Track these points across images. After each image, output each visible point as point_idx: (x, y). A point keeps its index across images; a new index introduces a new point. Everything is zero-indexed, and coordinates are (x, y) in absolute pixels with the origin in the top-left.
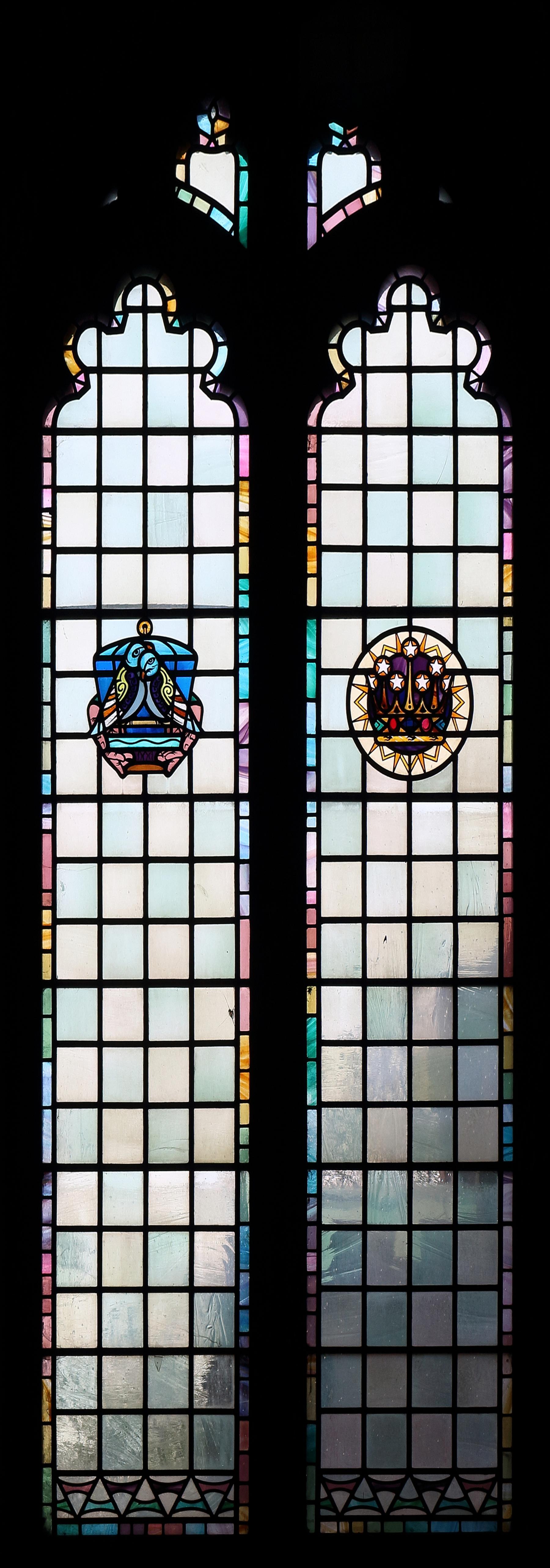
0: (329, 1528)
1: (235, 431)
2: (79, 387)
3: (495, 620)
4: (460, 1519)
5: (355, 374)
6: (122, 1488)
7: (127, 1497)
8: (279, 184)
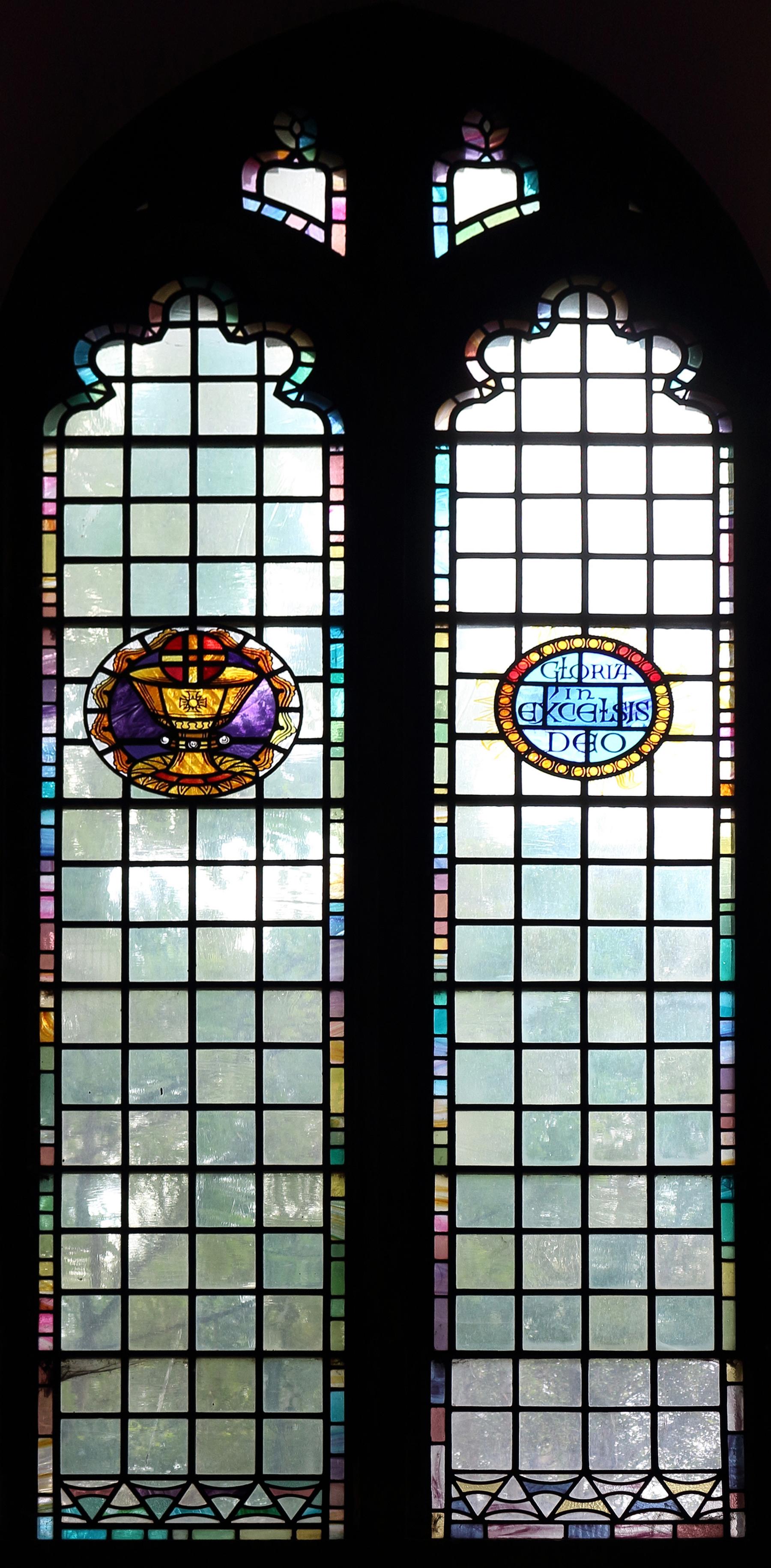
1: (714, 440)
7: (167, 1502)
8: (389, 202)
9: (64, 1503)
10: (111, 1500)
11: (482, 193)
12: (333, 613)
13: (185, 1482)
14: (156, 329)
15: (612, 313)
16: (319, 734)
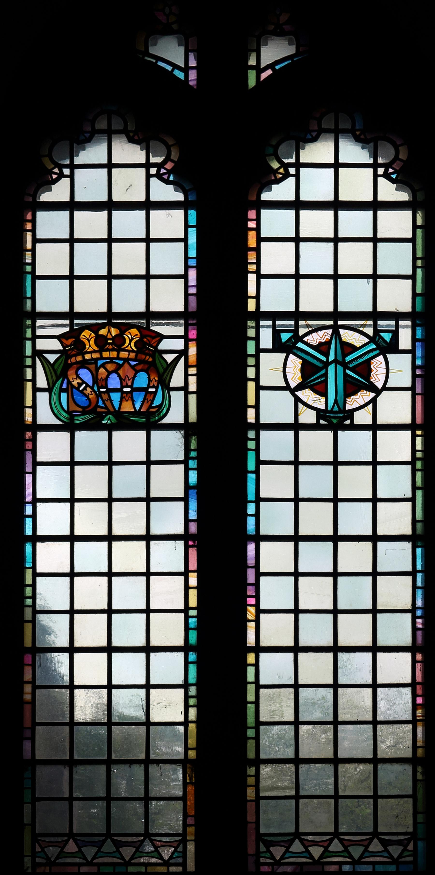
0: (265, 869)
4: (340, 864)
7: (400, 848)
8: (223, 57)
9: (261, 850)
10: (368, 848)
11: (273, 52)
12: (190, 310)
14: (87, 135)
15: (354, 125)
16: (182, 384)
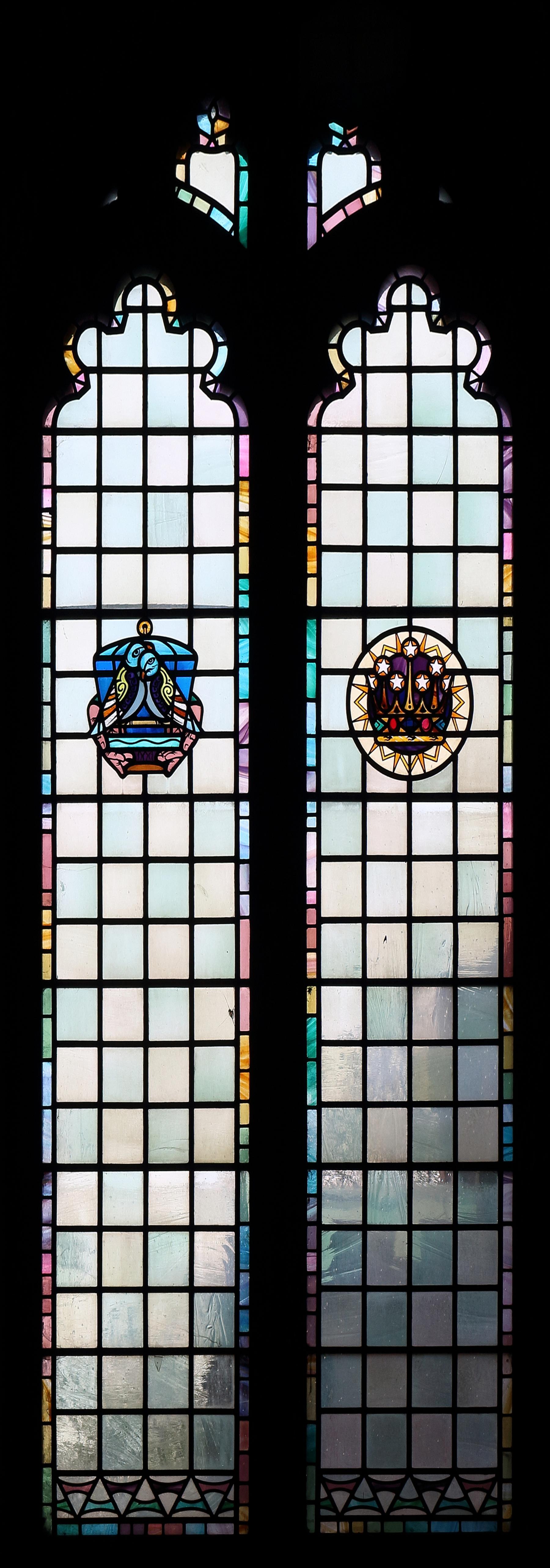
0: (329, 1528)
2: (79, 387)
3: (495, 620)
4: (460, 1519)
5: (355, 374)
6: (122, 1488)
7: (127, 1497)
8: (279, 184)
13: (448, 1476)
